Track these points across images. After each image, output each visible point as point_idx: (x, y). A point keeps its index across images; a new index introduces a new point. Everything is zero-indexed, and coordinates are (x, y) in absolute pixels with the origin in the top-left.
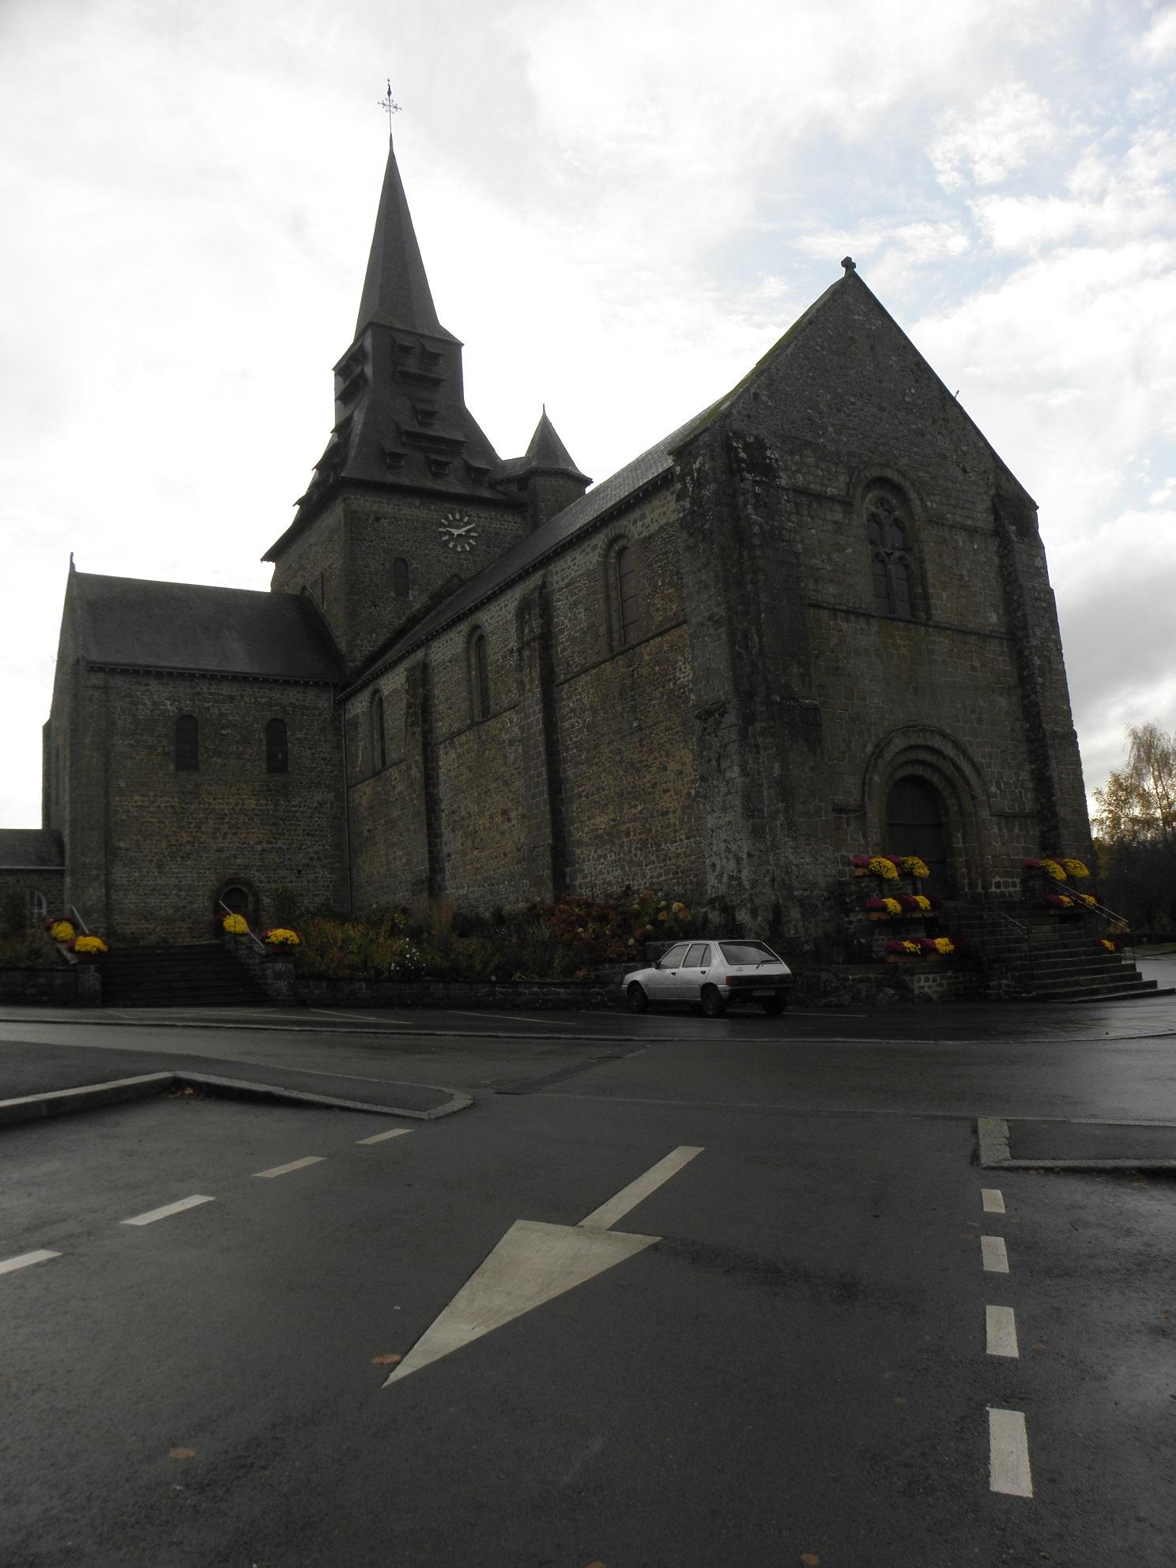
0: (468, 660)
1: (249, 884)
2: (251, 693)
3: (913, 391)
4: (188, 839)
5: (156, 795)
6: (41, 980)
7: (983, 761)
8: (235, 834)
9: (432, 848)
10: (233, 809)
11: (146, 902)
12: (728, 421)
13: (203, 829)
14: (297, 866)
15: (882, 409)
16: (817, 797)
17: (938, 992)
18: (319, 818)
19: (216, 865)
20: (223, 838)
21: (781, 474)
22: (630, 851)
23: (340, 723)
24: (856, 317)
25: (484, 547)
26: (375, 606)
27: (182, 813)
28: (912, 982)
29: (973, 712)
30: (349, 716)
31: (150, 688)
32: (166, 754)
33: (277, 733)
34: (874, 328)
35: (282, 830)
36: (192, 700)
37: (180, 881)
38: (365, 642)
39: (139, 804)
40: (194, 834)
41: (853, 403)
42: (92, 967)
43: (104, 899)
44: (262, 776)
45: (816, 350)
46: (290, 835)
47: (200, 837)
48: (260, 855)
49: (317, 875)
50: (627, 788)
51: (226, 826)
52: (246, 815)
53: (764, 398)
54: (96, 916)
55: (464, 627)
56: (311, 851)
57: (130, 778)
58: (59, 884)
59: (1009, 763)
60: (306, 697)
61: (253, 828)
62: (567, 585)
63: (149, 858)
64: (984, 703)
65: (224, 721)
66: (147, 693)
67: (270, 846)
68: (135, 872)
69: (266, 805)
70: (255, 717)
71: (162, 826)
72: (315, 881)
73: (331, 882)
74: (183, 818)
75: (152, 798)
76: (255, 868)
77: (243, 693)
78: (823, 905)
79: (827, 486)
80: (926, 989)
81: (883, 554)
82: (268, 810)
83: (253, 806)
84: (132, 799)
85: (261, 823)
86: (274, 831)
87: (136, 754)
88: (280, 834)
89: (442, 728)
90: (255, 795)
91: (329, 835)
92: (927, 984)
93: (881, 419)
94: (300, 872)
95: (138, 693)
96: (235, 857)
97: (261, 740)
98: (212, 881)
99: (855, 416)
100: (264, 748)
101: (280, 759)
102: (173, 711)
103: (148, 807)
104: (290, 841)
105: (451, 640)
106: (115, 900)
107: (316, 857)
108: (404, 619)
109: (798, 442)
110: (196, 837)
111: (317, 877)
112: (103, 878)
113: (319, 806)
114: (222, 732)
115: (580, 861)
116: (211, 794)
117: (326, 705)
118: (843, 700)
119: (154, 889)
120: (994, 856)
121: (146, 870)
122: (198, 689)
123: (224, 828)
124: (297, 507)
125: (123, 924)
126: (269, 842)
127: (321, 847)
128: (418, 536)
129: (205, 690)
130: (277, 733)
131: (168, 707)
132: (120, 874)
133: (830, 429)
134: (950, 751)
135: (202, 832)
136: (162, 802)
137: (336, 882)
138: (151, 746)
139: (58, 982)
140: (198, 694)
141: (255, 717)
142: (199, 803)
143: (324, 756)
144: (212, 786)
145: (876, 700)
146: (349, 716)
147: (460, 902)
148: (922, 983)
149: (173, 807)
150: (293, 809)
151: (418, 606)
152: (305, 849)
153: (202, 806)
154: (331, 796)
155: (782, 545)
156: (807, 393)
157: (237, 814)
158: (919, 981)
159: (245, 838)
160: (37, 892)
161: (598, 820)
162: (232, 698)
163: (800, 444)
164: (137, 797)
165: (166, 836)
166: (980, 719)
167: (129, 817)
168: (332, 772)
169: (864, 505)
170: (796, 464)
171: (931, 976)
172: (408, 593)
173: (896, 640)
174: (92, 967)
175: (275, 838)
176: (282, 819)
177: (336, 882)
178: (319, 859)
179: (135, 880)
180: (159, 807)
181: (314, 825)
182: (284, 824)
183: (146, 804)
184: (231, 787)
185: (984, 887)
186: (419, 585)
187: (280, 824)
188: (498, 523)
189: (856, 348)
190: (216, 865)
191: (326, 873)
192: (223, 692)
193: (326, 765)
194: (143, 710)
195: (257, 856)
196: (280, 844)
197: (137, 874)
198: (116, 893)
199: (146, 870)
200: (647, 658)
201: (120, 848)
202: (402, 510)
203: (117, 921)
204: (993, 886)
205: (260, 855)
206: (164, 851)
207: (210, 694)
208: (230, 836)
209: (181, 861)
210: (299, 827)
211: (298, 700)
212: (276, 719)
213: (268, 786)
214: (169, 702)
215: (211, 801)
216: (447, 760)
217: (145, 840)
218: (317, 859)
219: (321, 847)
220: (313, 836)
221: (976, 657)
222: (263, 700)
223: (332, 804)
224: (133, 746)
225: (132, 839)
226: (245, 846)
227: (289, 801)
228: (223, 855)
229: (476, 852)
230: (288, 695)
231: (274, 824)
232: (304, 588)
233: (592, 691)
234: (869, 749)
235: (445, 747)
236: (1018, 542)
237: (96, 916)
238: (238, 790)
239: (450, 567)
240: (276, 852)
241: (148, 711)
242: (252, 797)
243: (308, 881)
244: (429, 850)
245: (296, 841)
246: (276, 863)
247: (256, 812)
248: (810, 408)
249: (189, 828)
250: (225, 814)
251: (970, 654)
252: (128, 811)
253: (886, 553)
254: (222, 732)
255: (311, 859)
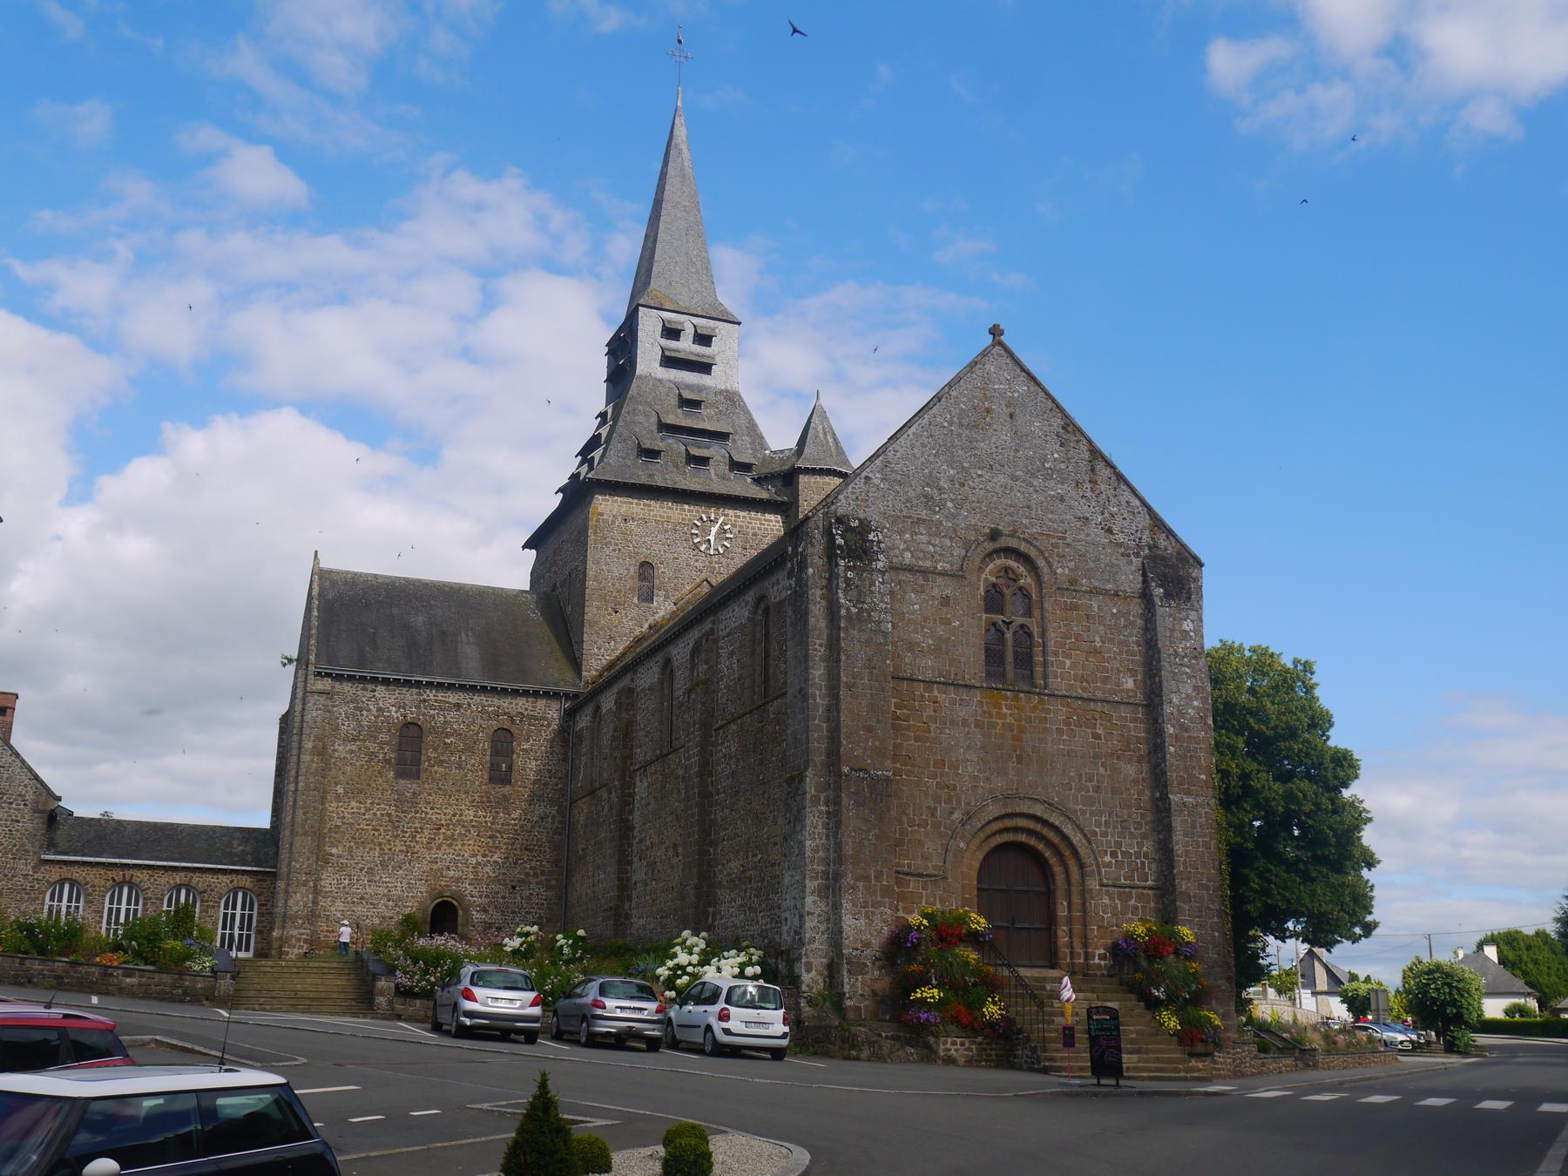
0: (663, 689)
1: (460, 896)
2: (479, 701)
3: (1056, 456)
4: (402, 848)
5: (372, 803)
6: (187, 983)
7: (1097, 830)
8: (450, 845)
9: (621, 876)
10: (450, 820)
11: (353, 911)
12: (833, 507)
13: (418, 839)
14: (512, 881)
15: (1014, 478)
16: (880, 863)
17: (966, 1056)
18: (538, 832)
19: (427, 876)
20: (437, 849)
21: (880, 557)
22: (750, 898)
23: (569, 734)
24: (997, 387)
25: (740, 550)
26: (616, 612)
27: (397, 821)
28: (938, 1044)
29: (1090, 779)
30: (577, 728)
31: (376, 694)
32: (387, 761)
33: (503, 741)
34: (1016, 395)
35: (500, 843)
36: (418, 707)
37: (389, 891)
38: (602, 650)
39: (355, 810)
40: (407, 844)
41: (980, 476)
42: (229, 975)
43: (311, 905)
44: (483, 787)
45: (944, 427)
46: (507, 849)
47: (414, 847)
48: (473, 867)
49: (532, 891)
50: (752, 837)
51: (441, 837)
52: (463, 826)
53: (876, 481)
54: (300, 922)
55: (660, 657)
56: (528, 866)
57: (348, 784)
58: (272, 886)
59: (1131, 832)
60: (536, 707)
61: (470, 840)
62: (728, 635)
63: (360, 866)
64: (1106, 770)
65: (449, 730)
66: (373, 699)
67: (485, 859)
68: (345, 879)
69: (485, 817)
70: (481, 726)
71: (376, 833)
72: (529, 898)
73: (546, 900)
74: (398, 826)
75: (368, 805)
76: (468, 882)
77: (471, 701)
78: (874, 964)
79: (937, 562)
80: (953, 1052)
81: (1001, 623)
82: (486, 822)
83: (472, 818)
84: (348, 805)
85: (478, 836)
86: (491, 844)
87: (357, 761)
88: (496, 848)
89: (641, 754)
90: (474, 806)
91: (548, 850)
92: (953, 1048)
93: (1011, 489)
94: (514, 887)
95: (364, 699)
96: (448, 868)
97: (485, 750)
98: (421, 893)
99: (981, 489)
100: (488, 758)
101: (504, 770)
102: (398, 718)
103: (364, 814)
104: (506, 855)
105: (651, 668)
106: (322, 906)
107: (532, 873)
108: (646, 626)
109: (911, 520)
110: (409, 846)
111: (531, 894)
112: (311, 883)
113: (540, 820)
114: (446, 740)
115: (720, 902)
116: (429, 803)
117: (555, 716)
118: (932, 769)
119: (362, 898)
120: (1100, 927)
121: (356, 878)
122: (425, 696)
123: (439, 839)
124: (560, 495)
125: (328, 931)
126: (484, 856)
127: (539, 863)
128: (667, 539)
129: (432, 697)
130: (503, 741)
131: (393, 713)
132: (329, 880)
133: (949, 504)
134: (1056, 820)
135: (417, 842)
136: (378, 810)
137: (551, 900)
138: (373, 753)
139: (200, 985)
140: (425, 701)
141: (481, 726)
142: (416, 812)
143: (550, 768)
144: (430, 795)
145: (970, 769)
146: (577, 728)
147: (640, 931)
148: (949, 1046)
149: (389, 815)
150: (513, 822)
151: (662, 613)
152: (522, 864)
153: (418, 815)
154: (554, 810)
155: (869, 626)
156: (926, 471)
157: (454, 825)
158: (945, 1043)
159: (461, 850)
160: (249, 893)
161: (732, 865)
162: (458, 706)
163: (912, 523)
164: (353, 804)
165: (380, 844)
166: (1098, 787)
167: (343, 823)
168: (557, 785)
169: (983, 576)
170: (905, 542)
171: (958, 1040)
172: (653, 599)
173: (1002, 709)
174: (229, 975)
175: (490, 852)
176: (500, 833)
177: (551, 900)
178: (535, 875)
179: (344, 887)
180: (375, 814)
181: (533, 840)
182: (502, 837)
183: (362, 811)
184: (450, 796)
185: (1086, 958)
186: (665, 590)
187: (497, 837)
188: (758, 522)
189: (991, 418)
190: (427, 876)
191: (542, 890)
192: (450, 700)
193: (550, 777)
194: (367, 716)
195: (470, 869)
196: (496, 858)
197: (347, 882)
198: (323, 900)
199: (356, 878)
200: (772, 716)
201: (331, 855)
202: (653, 511)
203: (321, 928)
204: (1097, 957)
205: (473, 867)
206: (376, 859)
207: (436, 701)
208: (444, 847)
209: (393, 871)
210: (517, 842)
211: (526, 709)
212: (503, 729)
213: (488, 797)
214: (394, 709)
215: (428, 810)
216: (641, 788)
217: (357, 848)
218: (533, 876)
219: (539, 863)
220: (531, 851)
221: (1101, 724)
222: (490, 709)
223: (554, 818)
224: (353, 752)
225: (345, 846)
226: (460, 858)
227: (509, 814)
228: (435, 867)
229: (654, 883)
230: (517, 704)
231: (491, 837)
232: (555, 586)
233: (737, 739)
234: (957, 816)
235: (641, 775)
236: (1162, 606)
237: (300, 922)
238: (457, 800)
239: (701, 571)
240: (491, 866)
241: (373, 718)
242: (470, 808)
243: (522, 898)
244: (619, 877)
245: (512, 855)
246: (490, 877)
247: (474, 823)
248: (928, 485)
249: (404, 837)
250: (442, 825)
251: (1093, 721)
252: (344, 817)
253: (1003, 621)
254: (446, 740)
255: (527, 875)
